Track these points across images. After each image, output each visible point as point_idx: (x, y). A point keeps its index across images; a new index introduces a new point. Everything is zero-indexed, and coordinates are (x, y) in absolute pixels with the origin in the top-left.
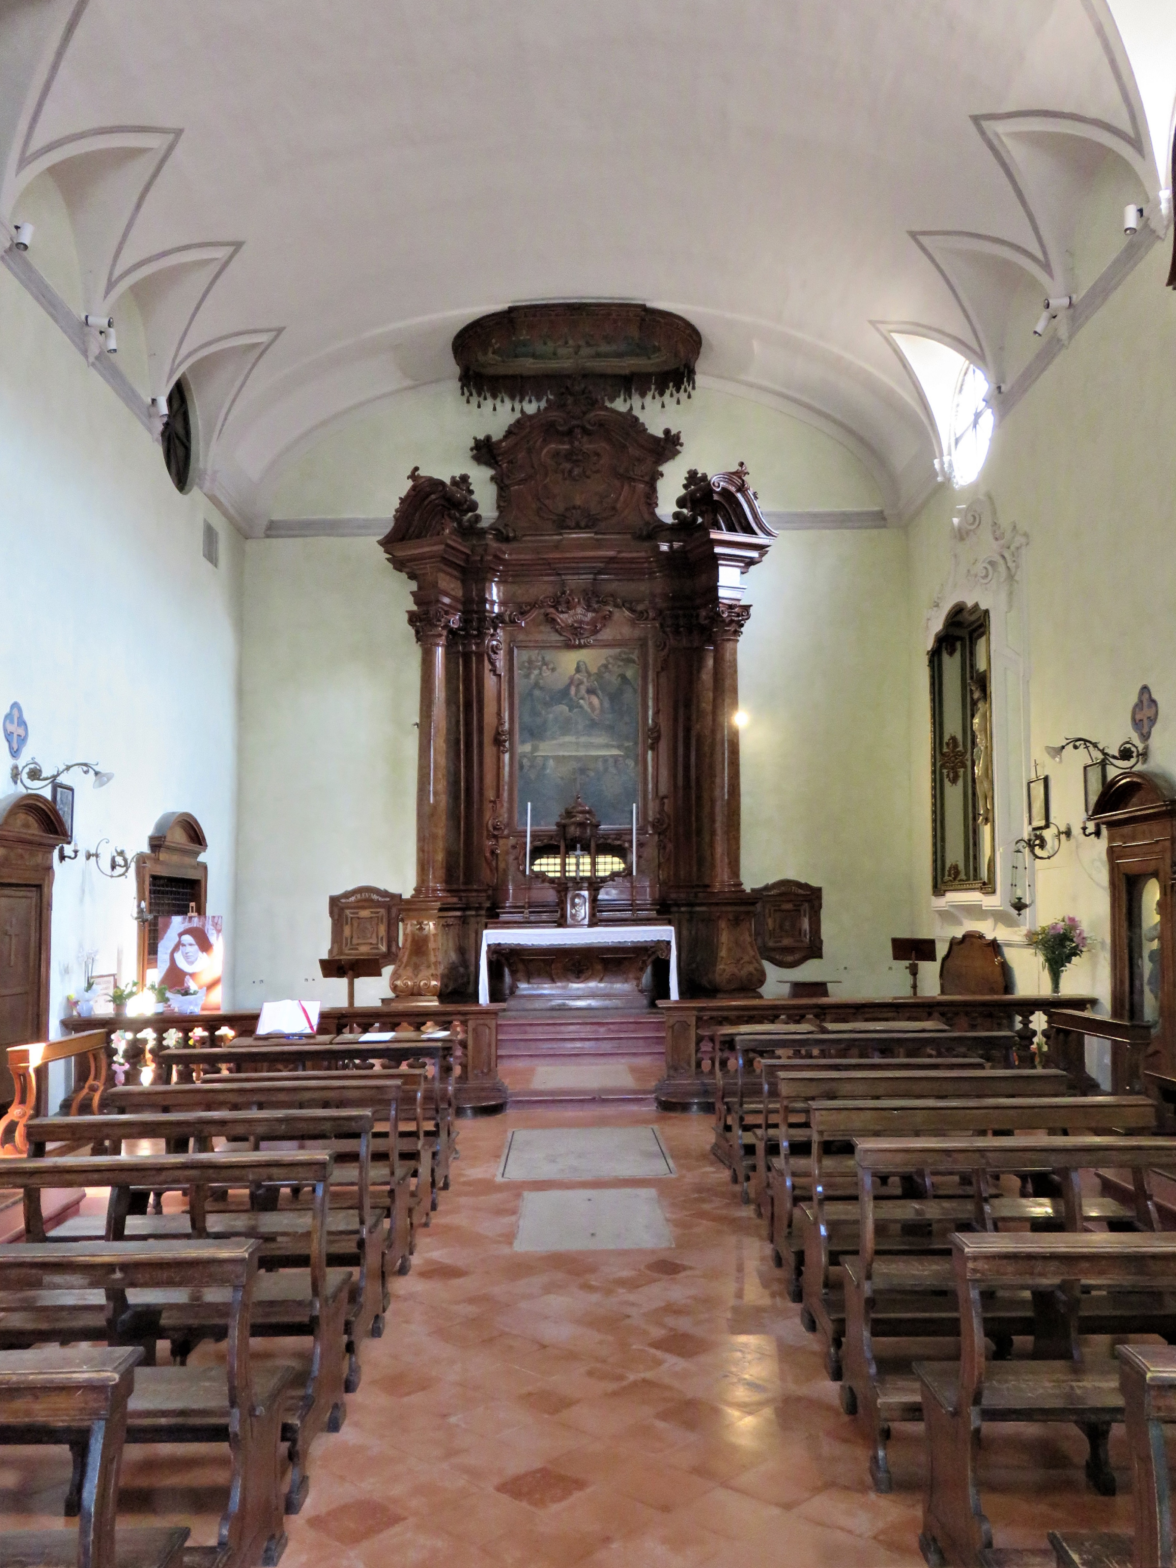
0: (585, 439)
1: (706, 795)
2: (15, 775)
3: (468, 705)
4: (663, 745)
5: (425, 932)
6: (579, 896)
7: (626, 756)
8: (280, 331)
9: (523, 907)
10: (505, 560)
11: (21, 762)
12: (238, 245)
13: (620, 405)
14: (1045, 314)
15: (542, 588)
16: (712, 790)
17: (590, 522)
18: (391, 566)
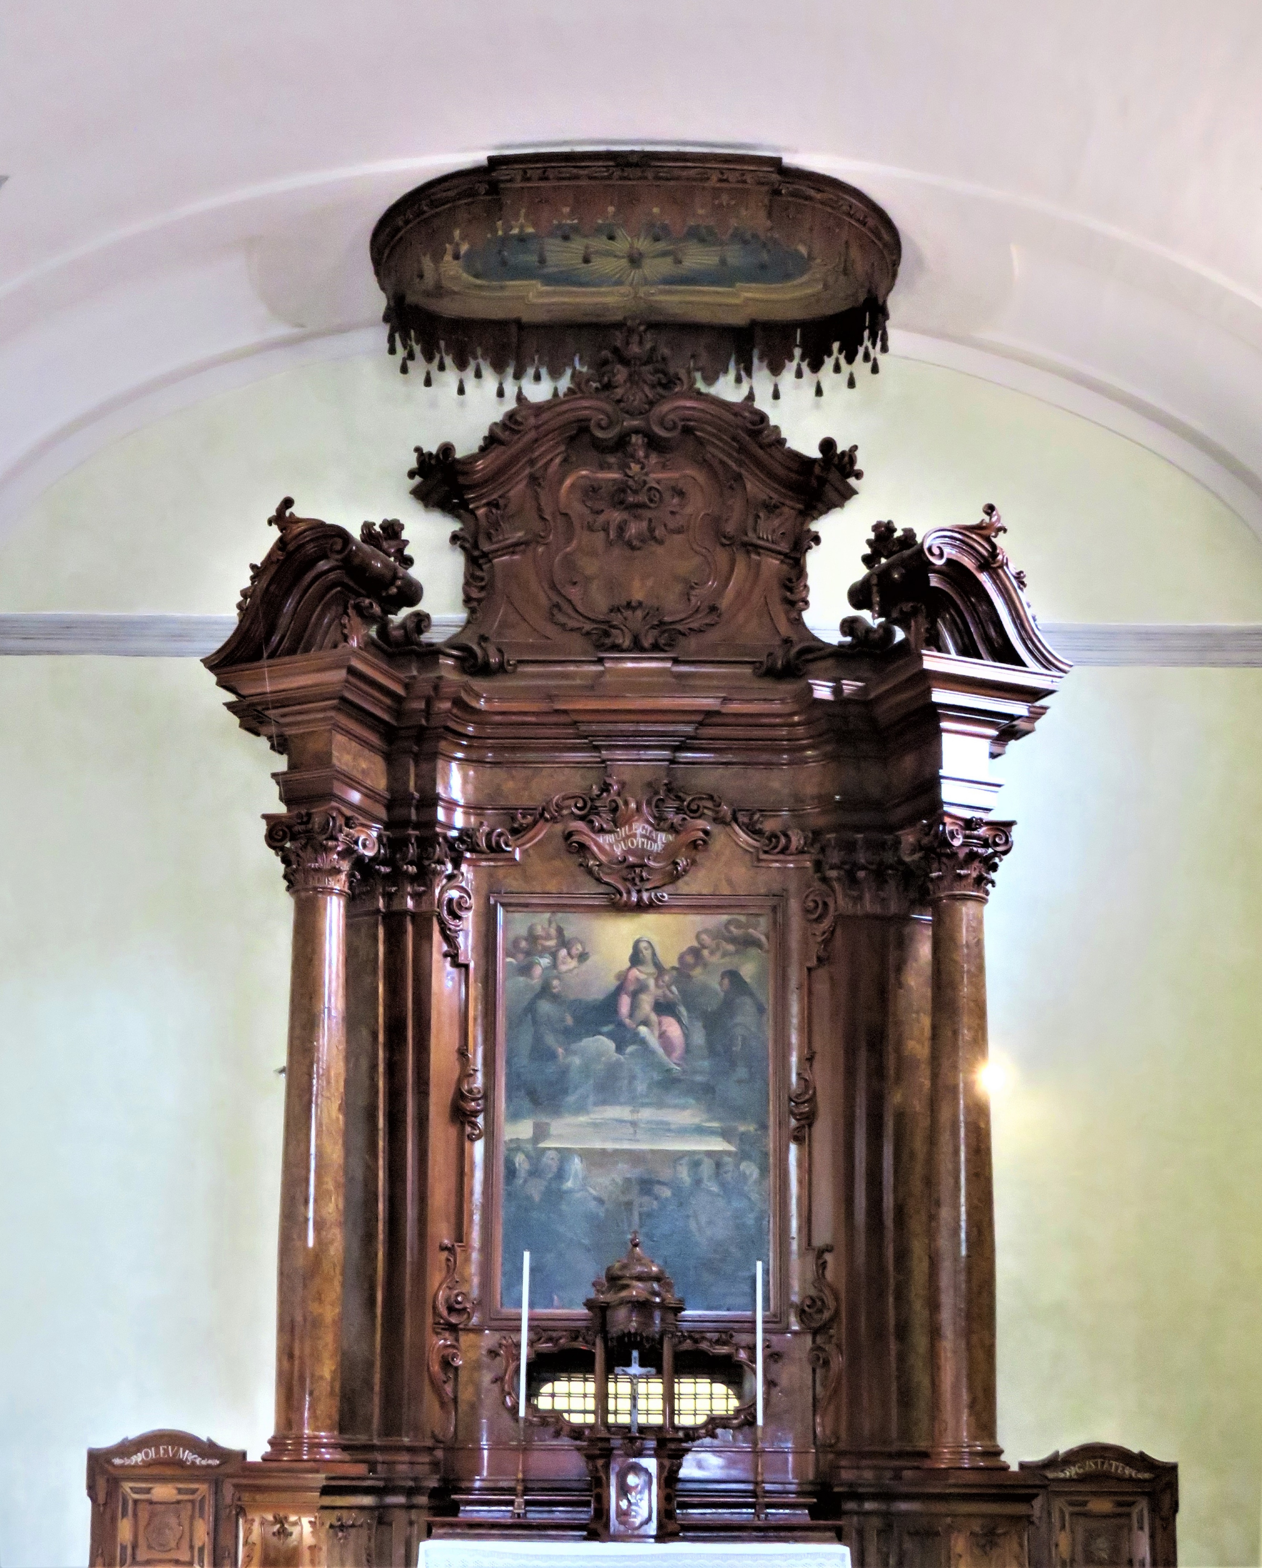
0: (654, 459)
1: (918, 1247)
3: (396, 1029)
4: (824, 1131)
5: (293, 1540)
6: (637, 1469)
7: (743, 1156)
9: (511, 1491)
10: (478, 712)
13: (727, 389)
15: (559, 777)
16: (931, 1234)
17: (664, 638)
18: (236, 720)
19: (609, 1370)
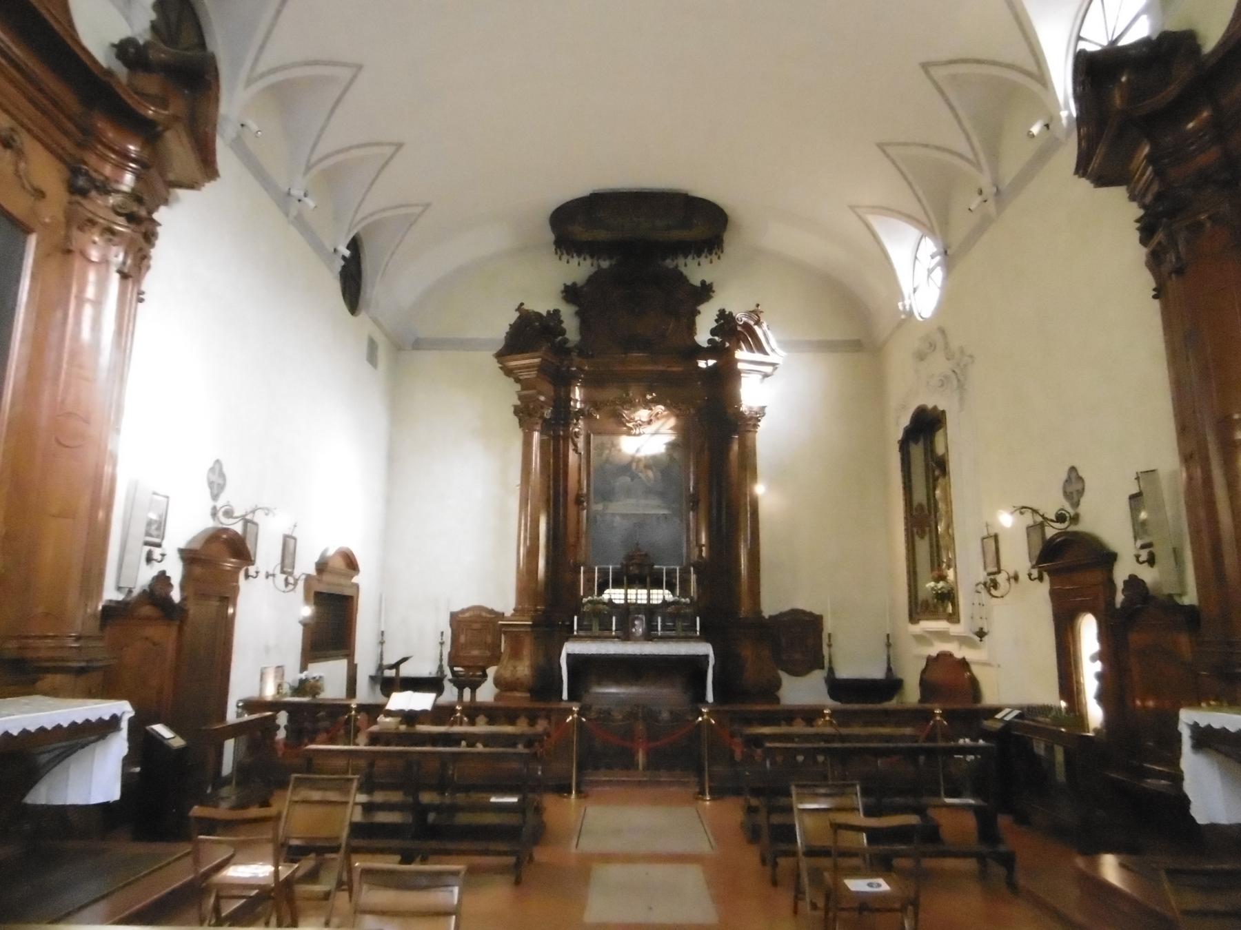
2: (214, 514)
4: (702, 506)
8: (428, 205)
11: (219, 504)
12: (399, 146)
14: (979, 199)
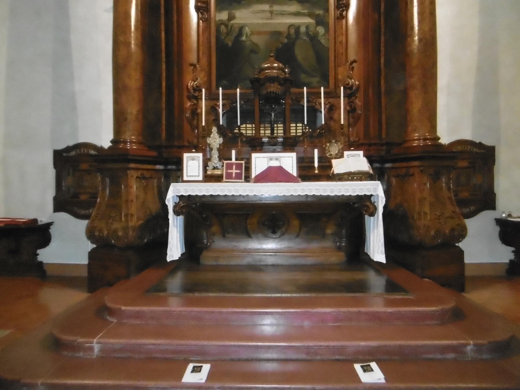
19: (260, 123)
